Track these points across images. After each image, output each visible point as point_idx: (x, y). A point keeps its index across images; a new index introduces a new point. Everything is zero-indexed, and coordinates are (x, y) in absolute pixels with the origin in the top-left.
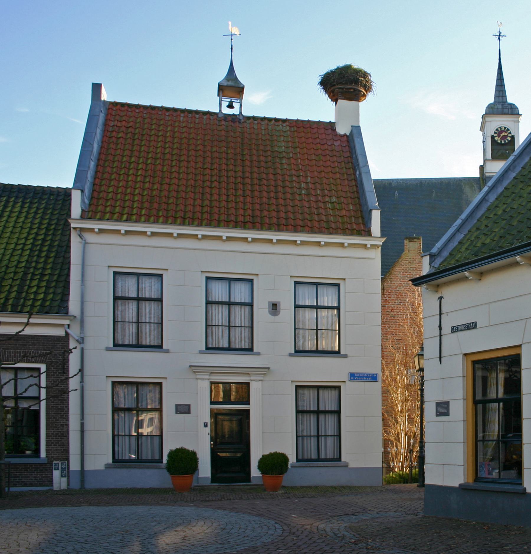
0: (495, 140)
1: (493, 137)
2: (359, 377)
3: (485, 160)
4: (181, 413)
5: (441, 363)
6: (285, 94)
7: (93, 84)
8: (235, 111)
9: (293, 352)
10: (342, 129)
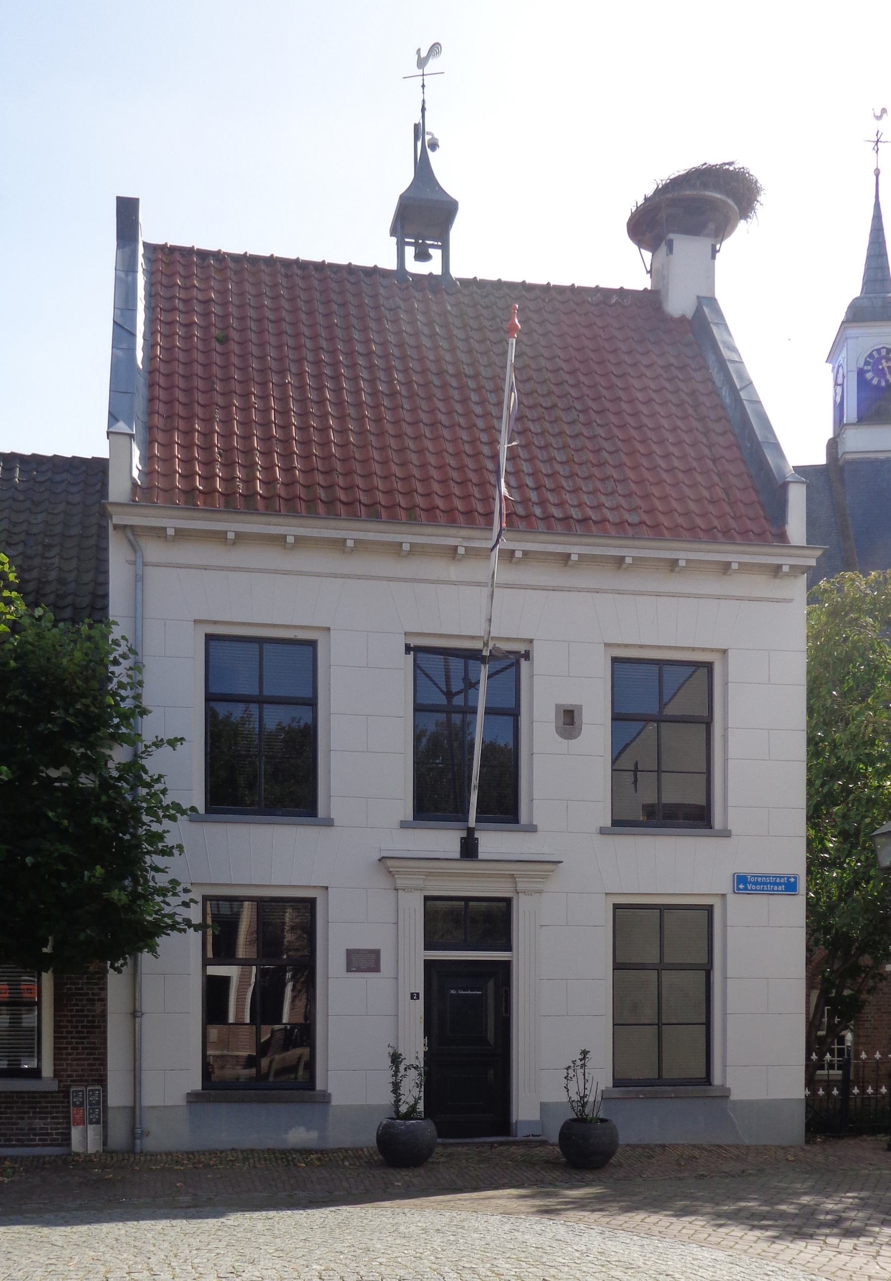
0: (866, 379)
1: (861, 373)
2: (756, 883)
4: (359, 970)
5: (560, 862)
6: (547, 227)
8: (433, 266)
9: (609, 824)
10: (679, 304)
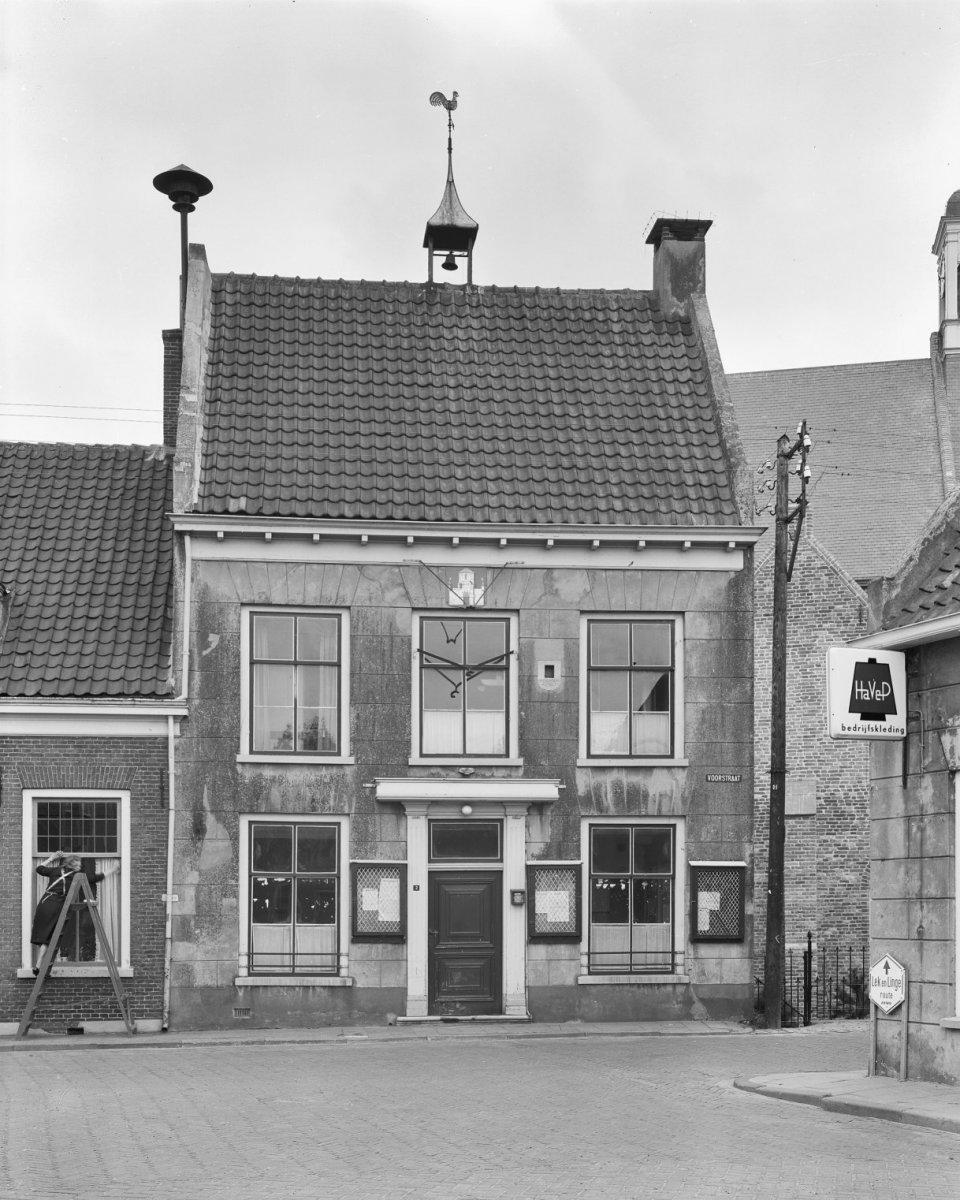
3: (944, 323)
7: (850, 712)
8: (457, 278)
